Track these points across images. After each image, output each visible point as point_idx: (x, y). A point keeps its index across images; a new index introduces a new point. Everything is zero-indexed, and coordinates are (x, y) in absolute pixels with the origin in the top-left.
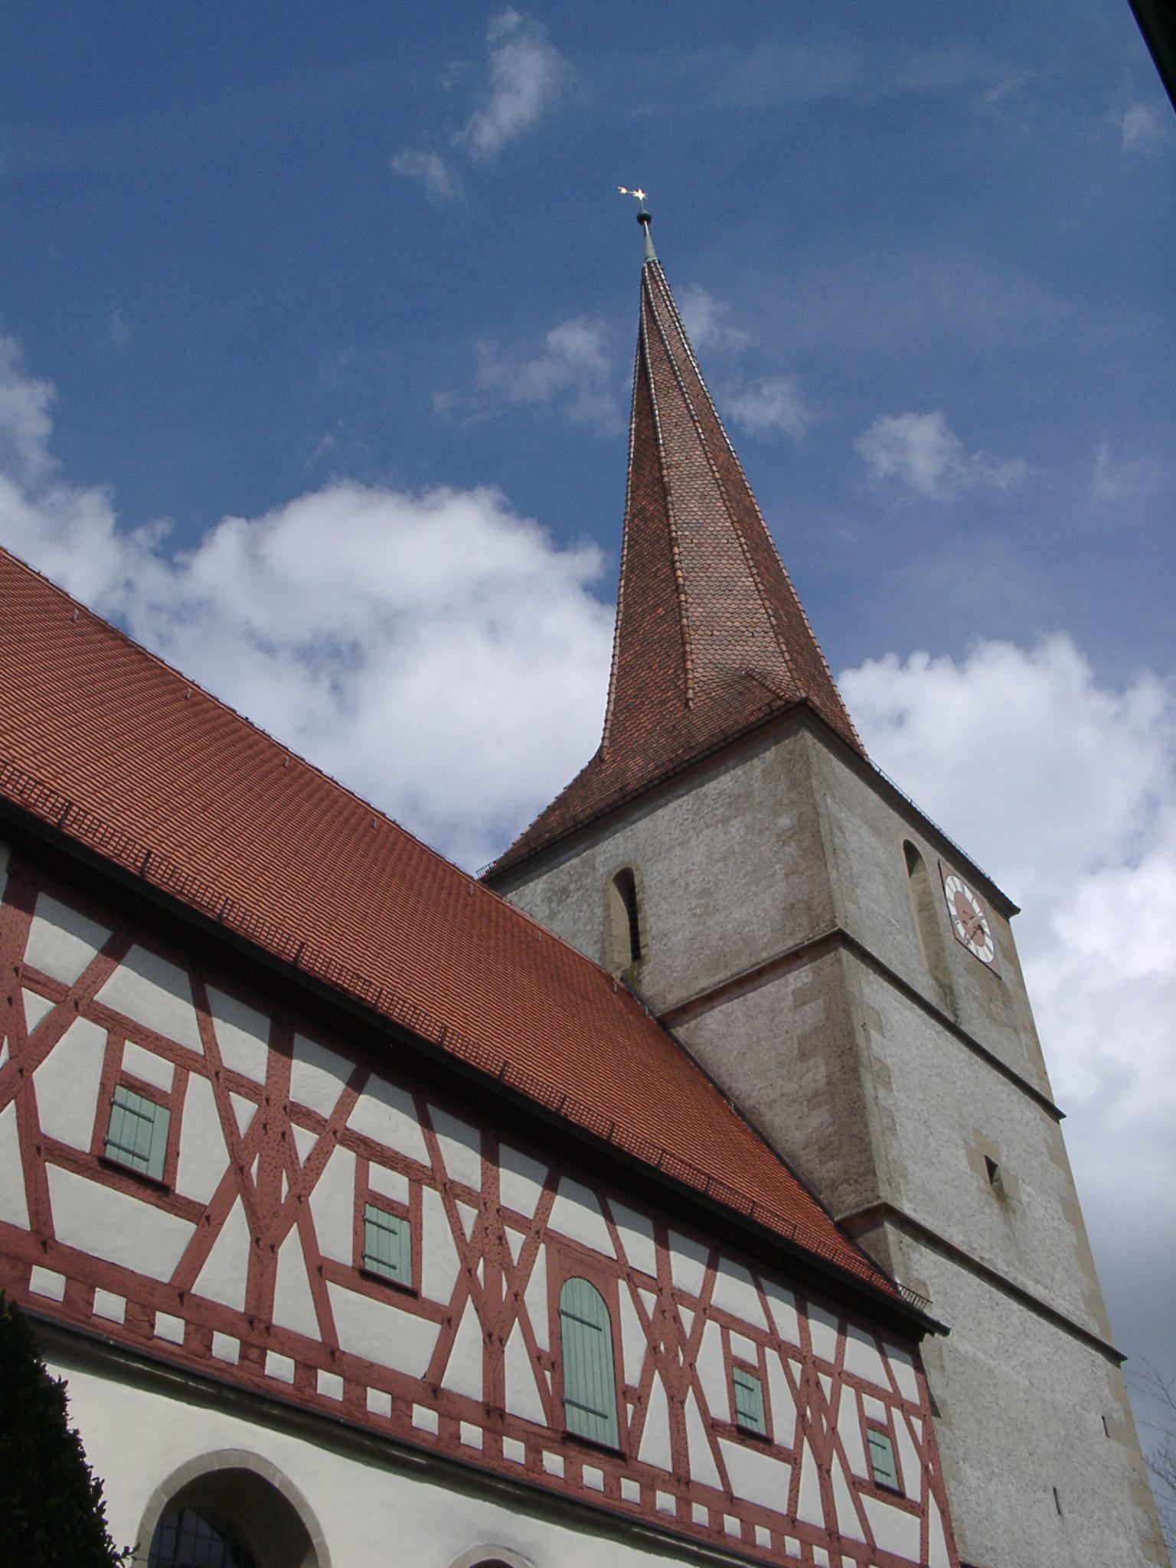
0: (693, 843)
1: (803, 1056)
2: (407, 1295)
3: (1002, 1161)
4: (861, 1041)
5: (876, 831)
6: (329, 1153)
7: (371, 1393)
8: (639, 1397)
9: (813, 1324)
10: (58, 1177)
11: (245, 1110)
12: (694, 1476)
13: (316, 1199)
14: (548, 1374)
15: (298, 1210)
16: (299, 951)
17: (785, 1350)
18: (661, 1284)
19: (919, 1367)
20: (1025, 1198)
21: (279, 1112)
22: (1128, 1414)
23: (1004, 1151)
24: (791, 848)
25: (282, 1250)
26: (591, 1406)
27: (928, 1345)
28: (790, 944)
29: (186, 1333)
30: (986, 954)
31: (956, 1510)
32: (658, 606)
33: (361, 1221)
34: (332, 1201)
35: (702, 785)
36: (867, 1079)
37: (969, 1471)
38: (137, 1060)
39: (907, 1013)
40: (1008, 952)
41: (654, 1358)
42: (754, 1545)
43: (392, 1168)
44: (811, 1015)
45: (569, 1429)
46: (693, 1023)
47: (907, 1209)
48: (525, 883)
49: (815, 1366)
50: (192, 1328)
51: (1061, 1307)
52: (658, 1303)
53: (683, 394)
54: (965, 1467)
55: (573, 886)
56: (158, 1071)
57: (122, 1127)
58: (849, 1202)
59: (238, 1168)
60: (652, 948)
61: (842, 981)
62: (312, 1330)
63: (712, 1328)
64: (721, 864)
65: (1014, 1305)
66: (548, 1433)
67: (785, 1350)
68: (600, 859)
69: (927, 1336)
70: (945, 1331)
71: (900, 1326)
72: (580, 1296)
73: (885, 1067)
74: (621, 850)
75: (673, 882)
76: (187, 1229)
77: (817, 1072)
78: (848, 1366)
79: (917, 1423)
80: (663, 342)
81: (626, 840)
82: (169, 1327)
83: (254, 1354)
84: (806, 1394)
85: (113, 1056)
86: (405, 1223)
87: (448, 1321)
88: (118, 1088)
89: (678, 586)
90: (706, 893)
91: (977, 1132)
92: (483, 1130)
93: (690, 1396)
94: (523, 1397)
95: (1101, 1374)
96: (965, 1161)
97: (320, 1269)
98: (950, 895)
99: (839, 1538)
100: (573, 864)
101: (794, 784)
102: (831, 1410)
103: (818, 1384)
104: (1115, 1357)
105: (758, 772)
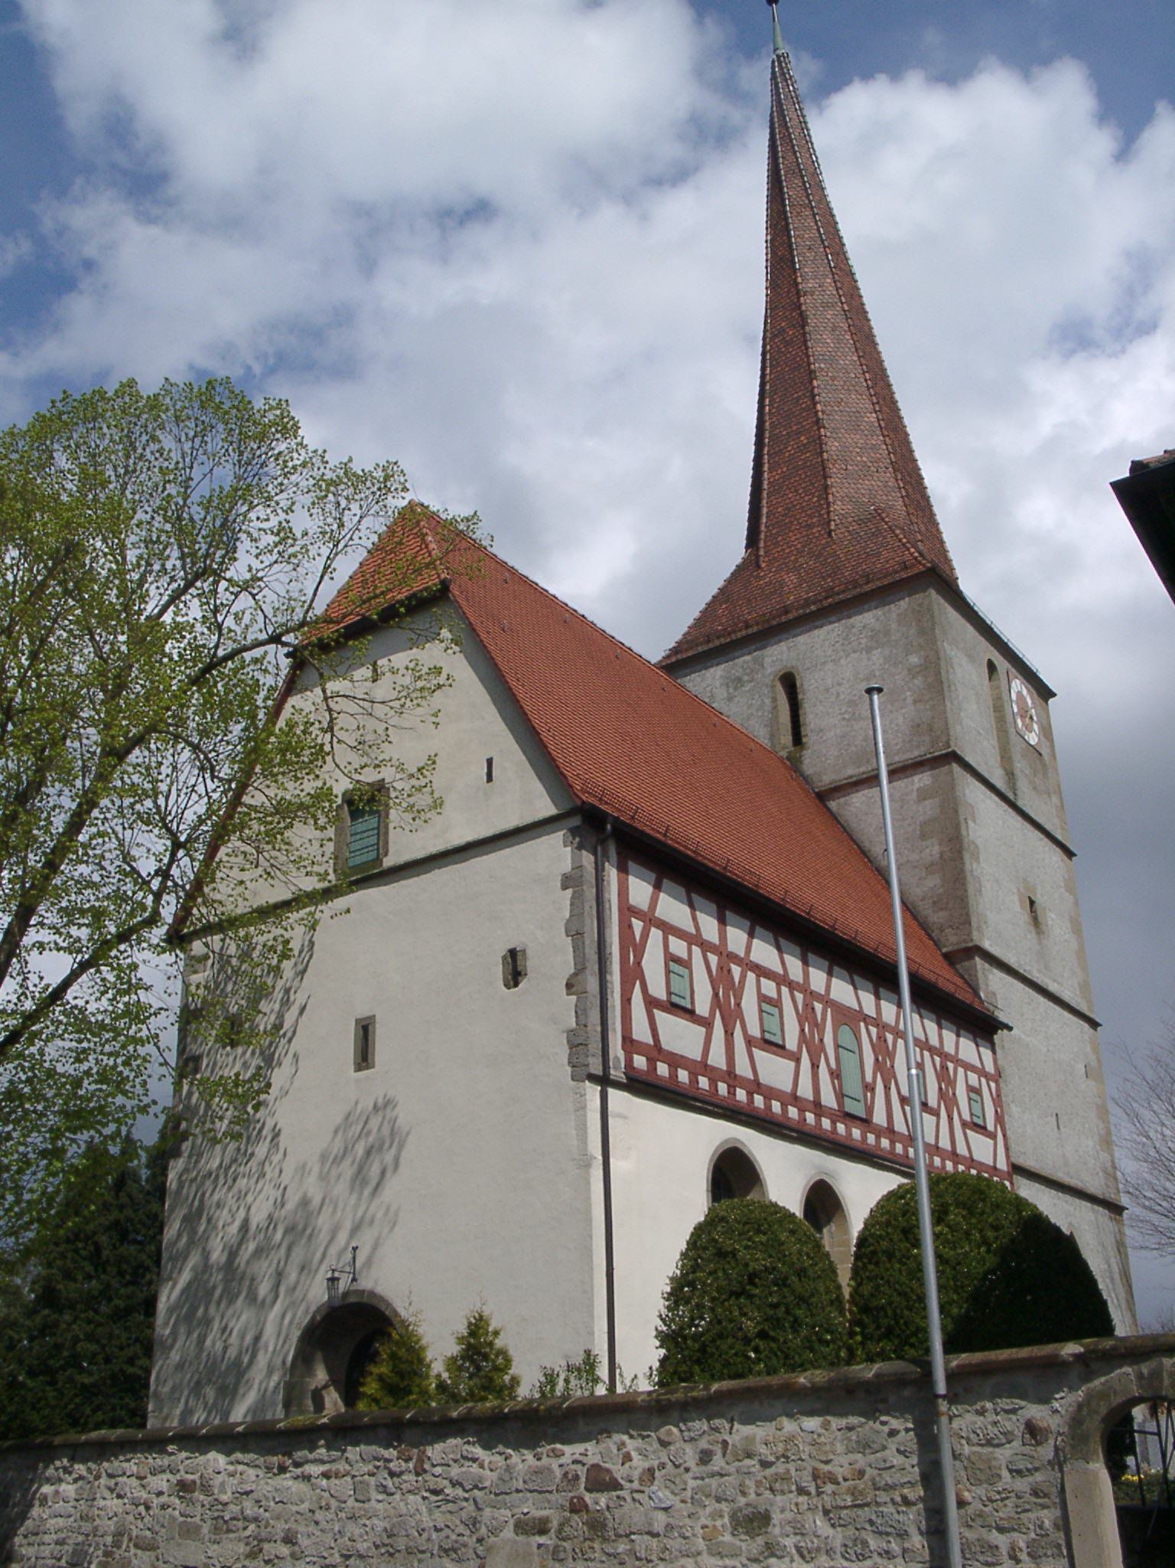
0: (843, 662)
1: (923, 836)
3: (1038, 900)
4: (964, 832)
9: (944, 1032)
12: (738, 1072)
19: (994, 1052)
22: (1099, 1061)
23: (1039, 892)
24: (918, 681)
27: (1000, 1036)
28: (915, 754)
30: (1033, 739)
32: (798, 433)
35: (849, 617)
36: (967, 857)
39: (988, 802)
41: (878, 1065)
44: (929, 808)
46: (842, 800)
47: (987, 945)
48: (706, 668)
51: (1066, 995)
53: (814, 215)
54: (1012, 1106)
55: (746, 678)
58: (952, 941)
60: (810, 738)
61: (952, 787)
63: (656, 934)
65: (1041, 999)
68: (768, 660)
70: (1010, 1029)
71: (983, 1026)
73: (977, 847)
74: (785, 656)
75: (827, 690)
77: (933, 850)
79: (993, 1085)
80: (795, 152)
81: (789, 649)
84: (721, 980)
89: (818, 420)
91: (1025, 880)
94: (829, 1099)
95: (1086, 1037)
98: (1014, 696)
100: (745, 660)
101: (922, 632)
102: (952, 1083)
104: (1094, 1024)
105: (894, 615)
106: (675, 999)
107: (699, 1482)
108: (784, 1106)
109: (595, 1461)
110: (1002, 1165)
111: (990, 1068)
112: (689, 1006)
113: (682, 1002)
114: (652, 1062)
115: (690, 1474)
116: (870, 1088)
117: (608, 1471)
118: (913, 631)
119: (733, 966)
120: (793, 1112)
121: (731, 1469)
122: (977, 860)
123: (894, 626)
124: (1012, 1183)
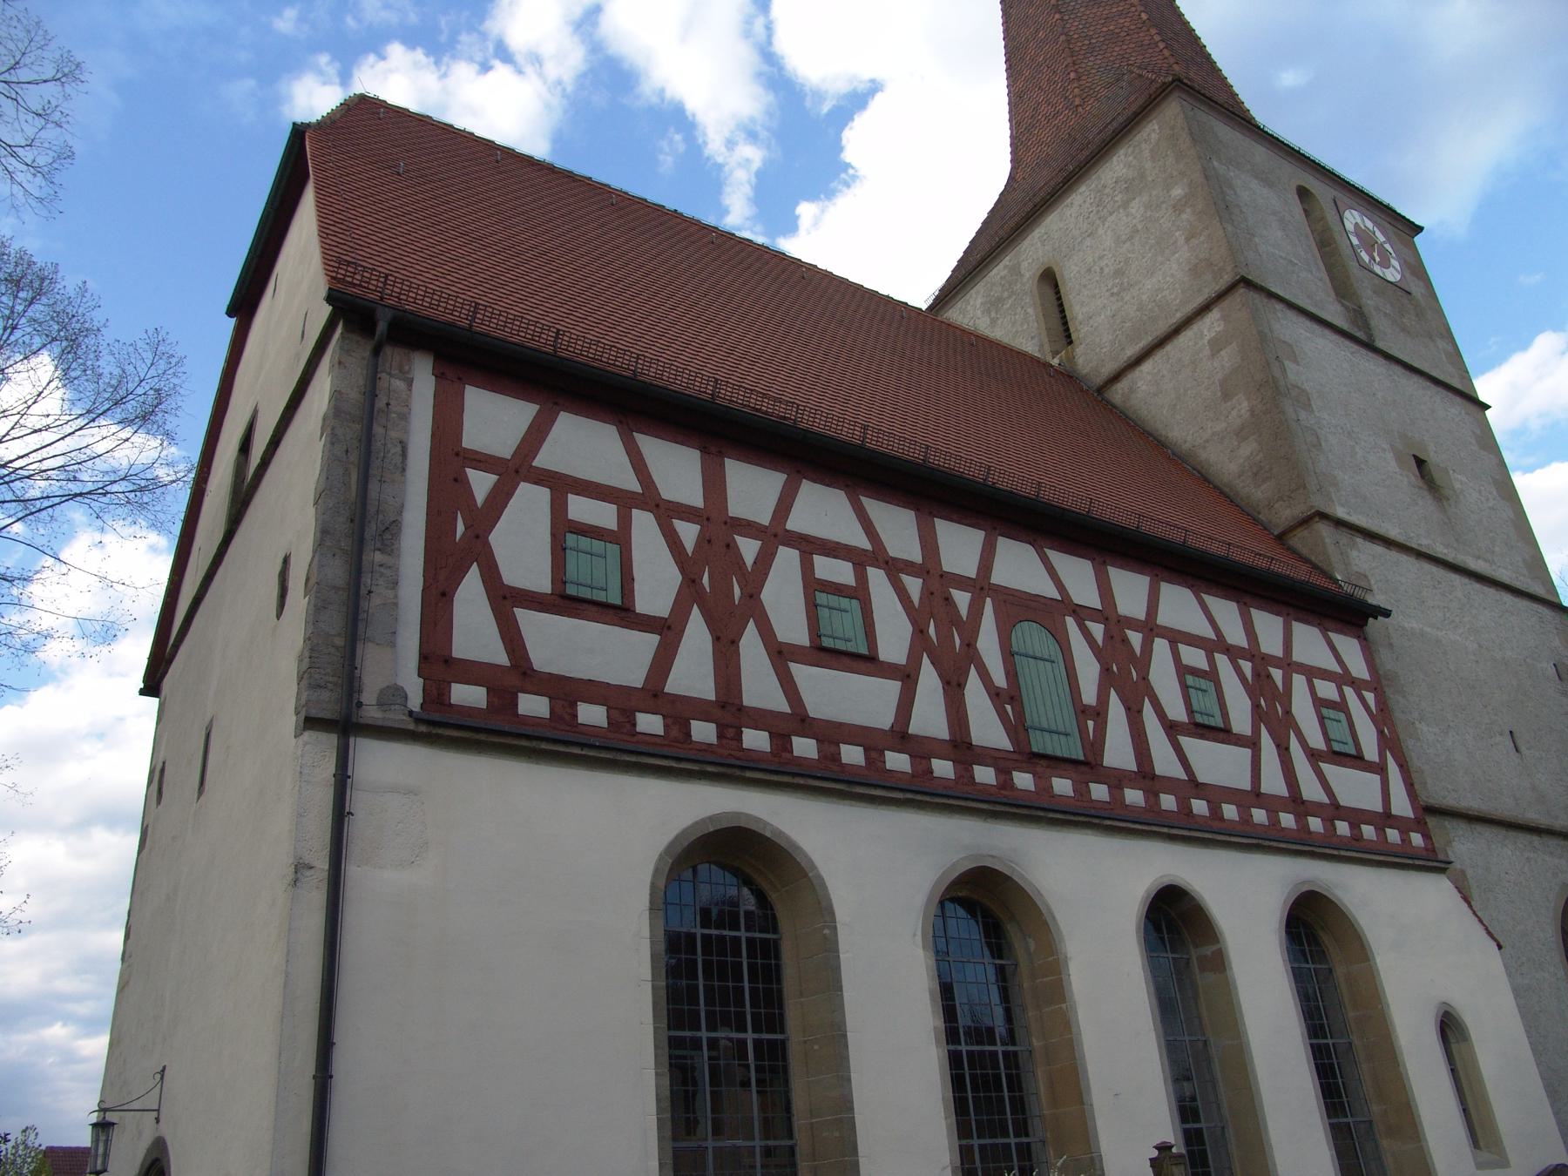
0: (1101, 231)
1: (1227, 396)
2: (867, 662)
3: (1433, 457)
5: (1267, 182)
6: (774, 554)
7: (844, 748)
8: (1099, 713)
10: (527, 619)
11: (914, 585)
13: (767, 595)
14: (1008, 707)
15: (753, 608)
16: (557, 338)
17: (1233, 653)
18: (1107, 614)
20: (1457, 486)
21: (718, 524)
25: (743, 643)
26: (1054, 728)
29: (666, 726)
30: (1393, 275)
31: (1415, 762)
33: (812, 608)
34: (783, 595)
37: (1425, 729)
38: (581, 509)
40: (1416, 268)
41: (1107, 679)
42: (1310, 832)
43: (835, 557)
45: (1035, 749)
49: (1262, 661)
50: (670, 721)
51: (1504, 575)
52: (1106, 631)
56: (603, 515)
57: (576, 567)
58: (1284, 515)
59: (690, 582)
60: (1079, 330)
62: (780, 704)
63: (1299, 681)
64: (1128, 244)
65: (1456, 579)
66: (1015, 756)
67: (1233, 653)
68: (1025, 265)
69: (1371, 620)
71: (1347, 612)
72: (1030, 636)
75: (1089, 270)
76: (653, 640)
77: (1241, 407)
78: (1297, 657)
82: (897, 761)
83: (731, 732)
84: (1259, 687)
85: (558, 509)
86: (854, 602)
87: (1253, 743)
88: (569, 536)
90: (1119, 273)
92: (917, 510)
93: (1147, 708)
94: (987, 729)
96: (1393, 463)
97: (780, 652)
98: (1349, 226)
99: (1303, 802)
103: (1269, 676)
105: (1146, 153)
106: (1336, 747)
108: (1380, 830)
110: (1401, 805)
111: (1359, 669)
112: (1353, 752)
113: (1212, 722)
114: (1329, 822)
119: (1129, 632)
120: (1393, 835)
122: (1307, 406)
123: (1148, 165)
124: (1426, 836)
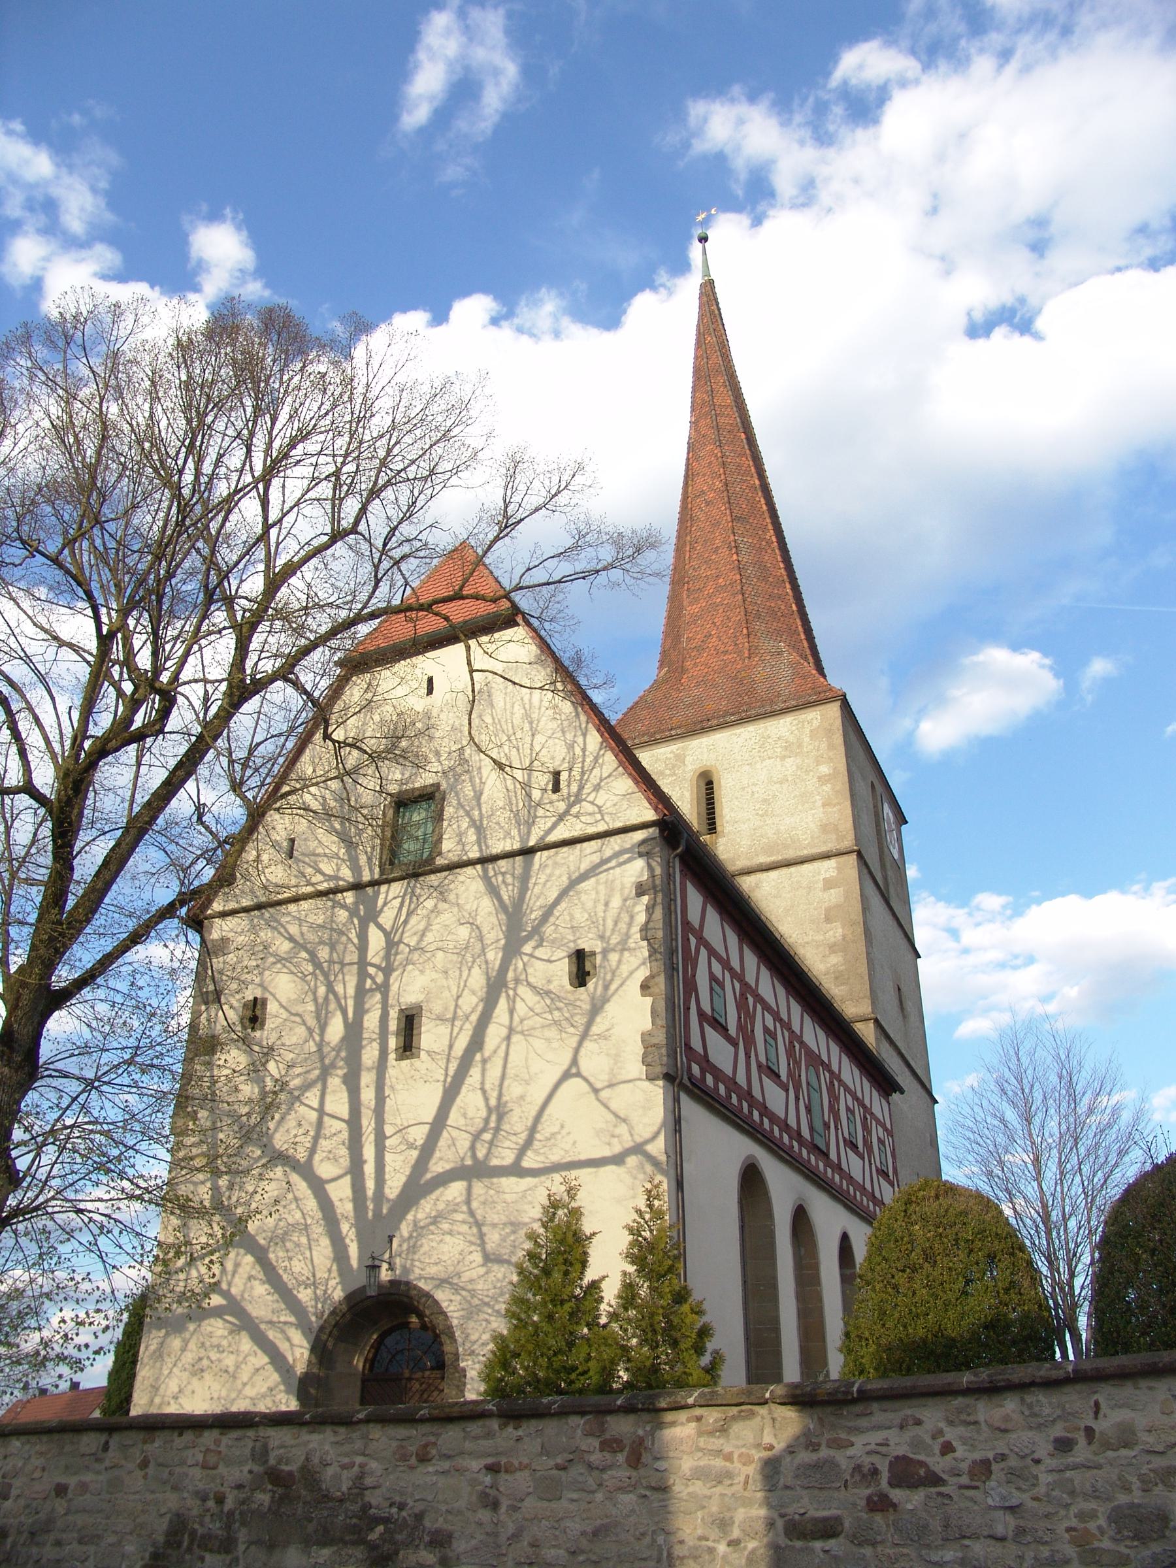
0: (758, 766)
1: (828, 920)
3: (903, 989)
24: (827, 788)
28: (823, 849)
55: (668, 772)
107: (1056, 1476)
109: (900, 1452)
115: (1042, 1467)
116: (827, 1126)
117: (922, 1464)
118: (824, 746)
121: (1100, 1459)
123: (807, 739)
